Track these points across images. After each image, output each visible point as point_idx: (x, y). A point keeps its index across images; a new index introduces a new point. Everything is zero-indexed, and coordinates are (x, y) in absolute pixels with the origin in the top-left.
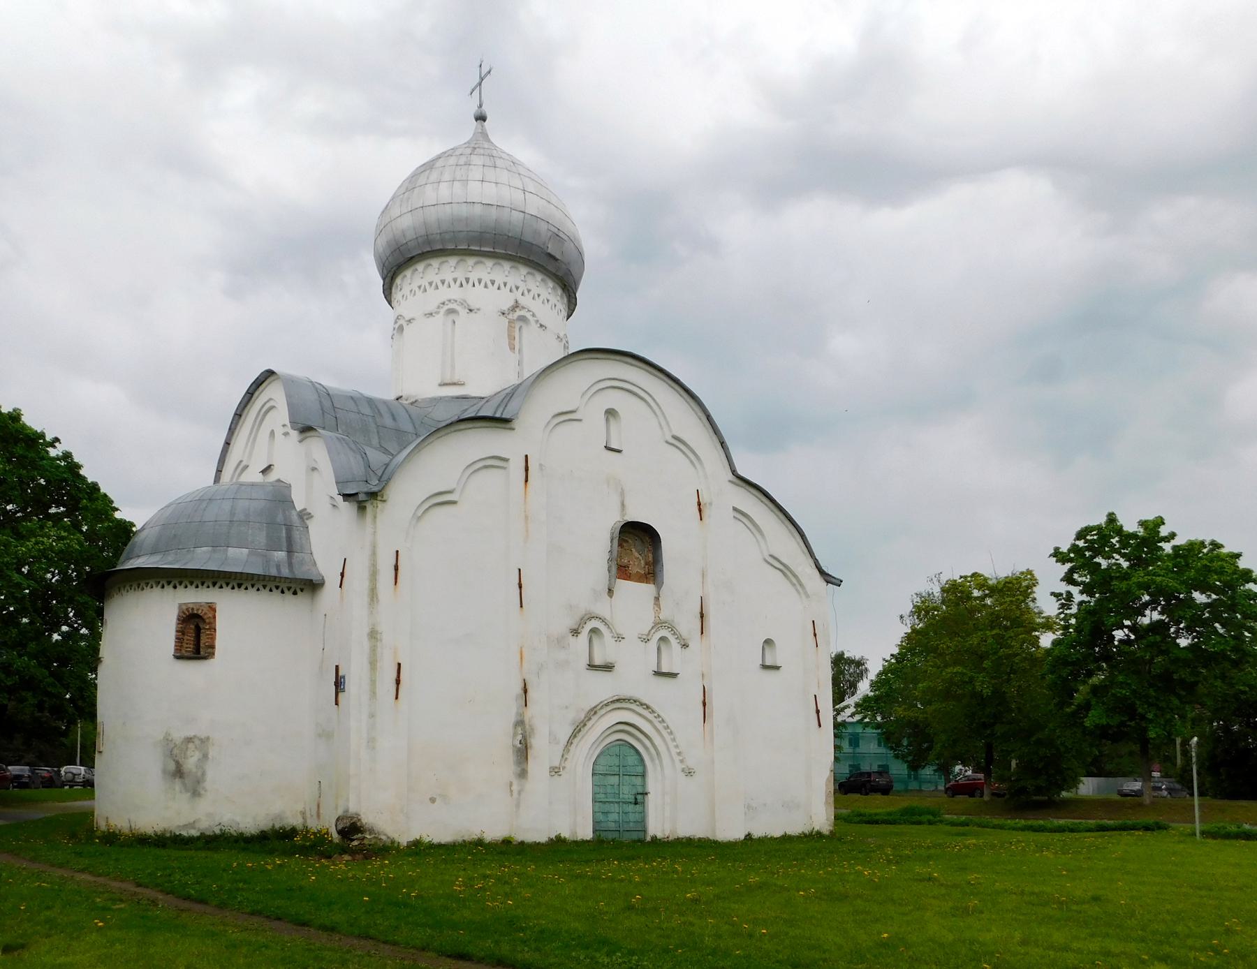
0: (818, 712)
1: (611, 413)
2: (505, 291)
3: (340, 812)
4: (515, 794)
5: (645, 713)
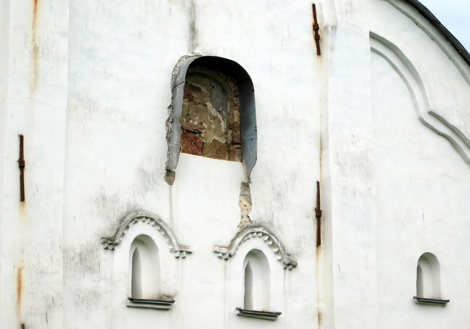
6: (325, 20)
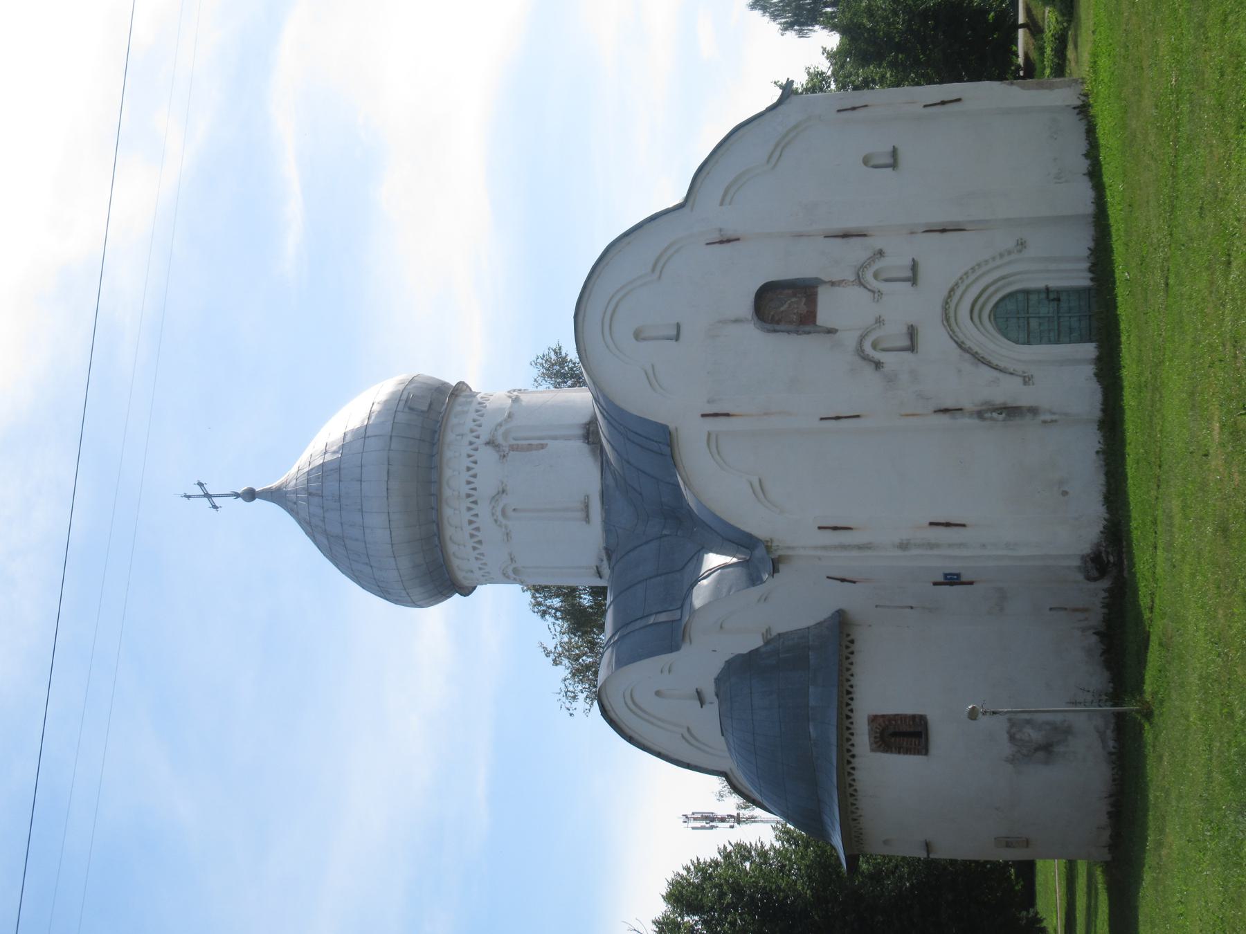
0: (943, 103)
1: (638, 336)
2: (477, 456)
3: (1080, 577)
4: (1054, 417)
5: (958, 292)
6: (716, 236)
